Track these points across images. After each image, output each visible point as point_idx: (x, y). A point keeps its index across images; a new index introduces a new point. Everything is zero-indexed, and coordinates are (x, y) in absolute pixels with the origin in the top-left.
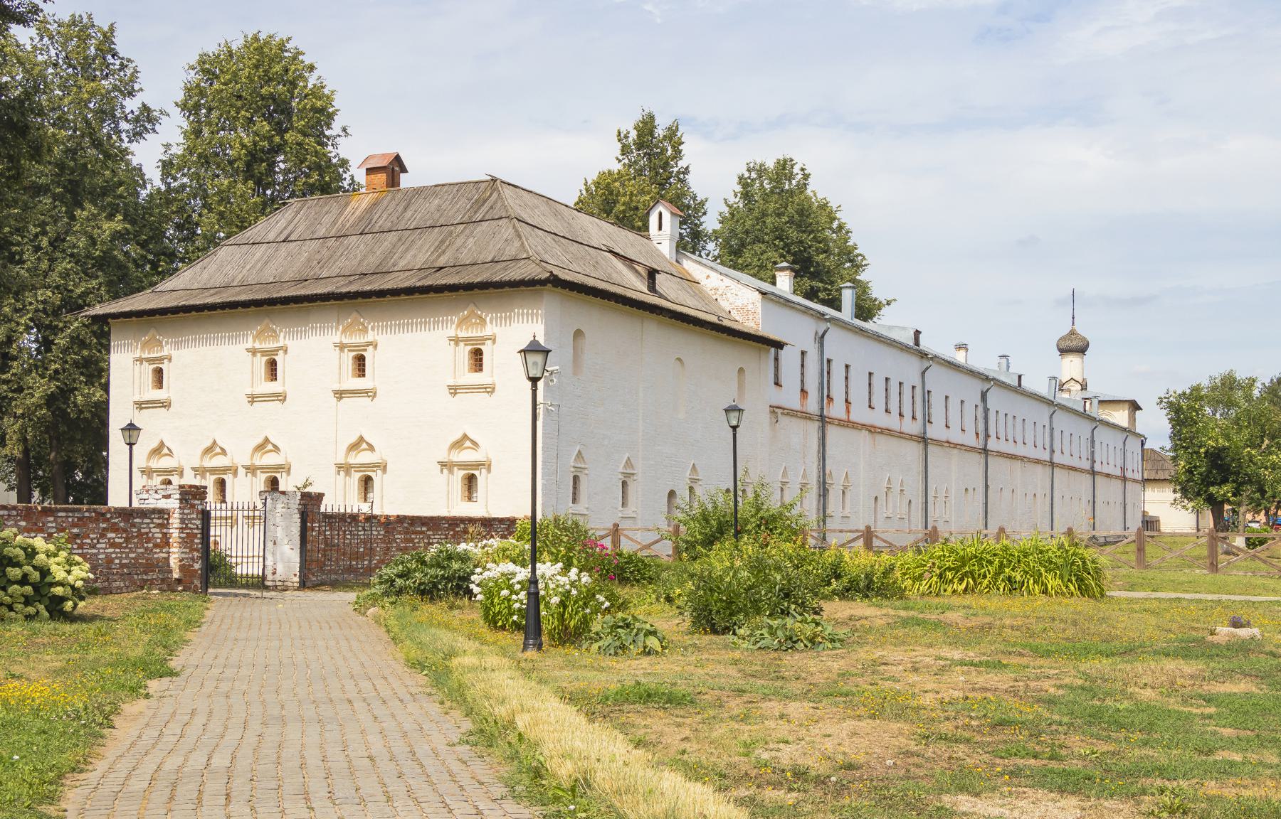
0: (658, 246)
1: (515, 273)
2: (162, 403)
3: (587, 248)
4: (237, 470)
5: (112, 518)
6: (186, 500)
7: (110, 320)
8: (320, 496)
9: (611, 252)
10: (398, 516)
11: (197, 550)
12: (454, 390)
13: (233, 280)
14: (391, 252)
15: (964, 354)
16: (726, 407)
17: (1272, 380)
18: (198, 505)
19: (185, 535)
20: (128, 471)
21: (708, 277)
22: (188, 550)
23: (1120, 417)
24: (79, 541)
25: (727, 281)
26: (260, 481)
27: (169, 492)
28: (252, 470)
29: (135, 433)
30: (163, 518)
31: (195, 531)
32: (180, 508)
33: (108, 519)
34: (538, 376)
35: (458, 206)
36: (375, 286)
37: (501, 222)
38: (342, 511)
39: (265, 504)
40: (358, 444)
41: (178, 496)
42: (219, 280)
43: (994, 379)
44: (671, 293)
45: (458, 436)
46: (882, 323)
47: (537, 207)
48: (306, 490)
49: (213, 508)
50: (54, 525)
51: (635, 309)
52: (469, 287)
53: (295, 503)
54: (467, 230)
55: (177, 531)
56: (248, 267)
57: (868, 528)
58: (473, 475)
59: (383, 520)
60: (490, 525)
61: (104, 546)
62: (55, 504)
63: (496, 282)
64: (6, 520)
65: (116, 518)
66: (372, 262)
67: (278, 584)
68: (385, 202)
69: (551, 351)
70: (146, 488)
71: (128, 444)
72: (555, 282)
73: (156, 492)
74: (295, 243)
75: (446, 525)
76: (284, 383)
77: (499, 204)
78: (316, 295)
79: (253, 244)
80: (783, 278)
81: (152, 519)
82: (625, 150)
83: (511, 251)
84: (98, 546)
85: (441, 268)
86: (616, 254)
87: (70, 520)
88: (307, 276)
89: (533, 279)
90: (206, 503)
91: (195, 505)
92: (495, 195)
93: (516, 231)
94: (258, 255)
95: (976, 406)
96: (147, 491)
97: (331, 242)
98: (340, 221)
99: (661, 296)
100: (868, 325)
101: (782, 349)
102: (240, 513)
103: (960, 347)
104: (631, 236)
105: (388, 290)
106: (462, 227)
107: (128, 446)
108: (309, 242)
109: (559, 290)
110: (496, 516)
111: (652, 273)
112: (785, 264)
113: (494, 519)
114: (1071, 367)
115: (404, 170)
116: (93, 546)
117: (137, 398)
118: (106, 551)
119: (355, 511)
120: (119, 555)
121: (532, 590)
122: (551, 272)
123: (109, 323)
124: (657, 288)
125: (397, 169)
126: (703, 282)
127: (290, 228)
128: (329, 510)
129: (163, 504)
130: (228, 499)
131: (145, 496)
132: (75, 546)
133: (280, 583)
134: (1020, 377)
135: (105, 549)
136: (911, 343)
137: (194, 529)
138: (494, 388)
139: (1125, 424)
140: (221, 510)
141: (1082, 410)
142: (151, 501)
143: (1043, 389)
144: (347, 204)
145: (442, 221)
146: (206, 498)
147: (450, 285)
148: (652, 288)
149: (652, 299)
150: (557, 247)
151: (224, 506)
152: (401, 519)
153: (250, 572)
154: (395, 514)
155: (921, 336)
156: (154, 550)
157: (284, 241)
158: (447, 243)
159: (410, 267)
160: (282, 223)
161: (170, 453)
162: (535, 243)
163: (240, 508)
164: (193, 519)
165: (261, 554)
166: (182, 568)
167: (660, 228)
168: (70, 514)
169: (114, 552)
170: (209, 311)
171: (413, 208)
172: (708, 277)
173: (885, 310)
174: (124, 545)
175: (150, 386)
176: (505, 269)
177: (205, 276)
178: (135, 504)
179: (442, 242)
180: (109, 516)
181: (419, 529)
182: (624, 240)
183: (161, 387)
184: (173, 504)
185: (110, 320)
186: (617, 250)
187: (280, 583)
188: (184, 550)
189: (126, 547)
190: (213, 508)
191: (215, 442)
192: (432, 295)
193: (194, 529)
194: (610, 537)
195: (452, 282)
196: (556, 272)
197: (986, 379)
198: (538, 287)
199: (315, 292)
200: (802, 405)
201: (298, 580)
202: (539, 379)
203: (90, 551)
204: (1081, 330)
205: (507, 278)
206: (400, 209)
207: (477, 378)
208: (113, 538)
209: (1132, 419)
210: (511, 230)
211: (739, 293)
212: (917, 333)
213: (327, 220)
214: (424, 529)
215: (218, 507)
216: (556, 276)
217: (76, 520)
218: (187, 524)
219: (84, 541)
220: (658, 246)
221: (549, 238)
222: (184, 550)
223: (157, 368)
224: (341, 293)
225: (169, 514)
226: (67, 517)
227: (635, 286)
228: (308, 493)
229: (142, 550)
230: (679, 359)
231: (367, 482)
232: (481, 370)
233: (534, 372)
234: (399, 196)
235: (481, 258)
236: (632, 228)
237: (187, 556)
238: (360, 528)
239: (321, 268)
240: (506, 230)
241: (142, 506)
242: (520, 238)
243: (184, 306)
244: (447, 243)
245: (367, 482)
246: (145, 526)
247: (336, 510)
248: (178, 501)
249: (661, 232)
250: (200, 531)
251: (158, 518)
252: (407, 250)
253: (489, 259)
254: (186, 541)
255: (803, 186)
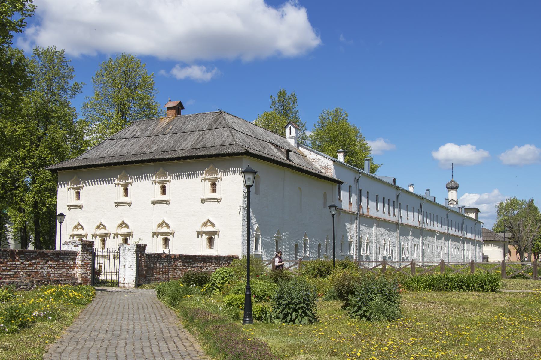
0: (290, 141)
1: (230, 150)
2: (79, 206)
3: (260, 141)
4: (110, 235)
5: (51, 255)
6: (85, 247)
7: (58, 171)
8: (145, 246)
9: (270, 143)
10: (179, 255)
11: (90, 270)
12: (203, 201)
13: (110, 154)
14: (177, 142)
15: (412, 188)
16: (330, 205)
17: (529, 200)
18: (90, 250)
19: (83, 263)
20: (61, 235)
21: (311, 154)
22: (85, 270)
23: (473, 215)
24: (35, 266)
25: (319, 156)
26: (120, 239)
27: (77, 244)
28: (116, 235)
29: (63, 217)
30: (74, 256)
31: (89, 261)
32: (82, 251)
33: (49, 256)
34: (251, 184)
35: (206, 123)
36: (170, 156)
37: (224, 129)
38: (155, 252)
39: (119, 249)
40: (163, 224)
41: (81, 246)
42: (104, 154)
43: (425, 199)
44: (295, 159)
45: (205, 220)
46: (378, 174)
47: (239, 123)
48: (139, 243)
49: (97, 251)
50: (24, 258)
51: (281, 166)
52: (210, 156)
53: (134, 249)
54: (210, 133)
55: (80, 261)
56: (116, 149)
57: (473, 261)
58: (212, 237)
59: (172, 257)
60: (219, 260)
61: (47, 268)
62: (36, 249)
63: (222, 154)
64: (1, 256)
65: (52, 255)
66: (169, 146)
67: (126, 285)
68: (175, 121)
69: (257, 172)
70: (67, 242)
71: (59, 222)
72: (248, 153)
73: (71, 244)
74: (136, 139)
75: (200, 259)
76: (131, 198)
77: (224, 121)
78: (145, 160)
79: (119, 139)
80: (340, 156)
81: (69, 256)
82: (273, 104)
83: (228, 141)
84: (44, 268)
85: (199, 148)
86: (273, 144)
87: (31, 256)
88: (141, 152)
89: (238, 152)
90: (94, 249)
91: (88, 250)
92: (222, 118)
93: (231, 132)
94: (121, 144)
95: (419, 210)
96: (67, 243)
97: (152, 138)
98: (156, 130)
99: (291, 161)
100: (373, 175)
101: (342, 184)
102: (111, 253)
103: (410, 186)
104: (279, 137)
105: (176, 158)
106: (208, 131)
107: (60, 223)
108: (142, 138)
109: (249, 157)
110: (222, 255)
111: (288, 151)
112: (341, 150)
113: (221, 256)
114: (452, 195)
115: (183, 108)
116: (42, 268)
117: (69, 204)
118: (48, 270)
119: (162, 253)
120: (54, 272)
121: (248, 293)
122: (246, 150)
123: (57, 173)
124: (290, 158)
125: (180, 107)
126: (309, 156)
127: (134, 132)
128: (149, 252)
129: (74, 249)
130: (106, 248)
131: (67, 246)
132: (34, 268)
133: (127, 285)
134: (435, 198)
135: (47, 269)
136: (392, 183)
137: (88, 260)
138: (221, 200)
139: (474, 218)
140: (103, 252)
141: (459, 212)
142: (69, 248)
143: (443, 203)
144: (159, 122)
145: (199, 129)
146: (93, 246)
147: (204, 155)
148: (288, 157)
149: (288, 162)
150: (248, 140)
151: (104, 250)
152: (181, 256)
153: (113, 279)
154: (178, 254)
155: (396, 181)
156: (70, 270)
157: (132, 138)
158: (201, 138)
159: (185, 148)
160: (131, 130)
161: (82, 228)
162: (239, 138)
163: (111, 251)
164: (88, 256)
165: (118, 271)
166: (82, 278)
167: (290, 134)
168: (32, 254)
169: (51, 271)
170: (100, 167)
171: (186, 124)
172: (311, 154)
173: (379, 169)
174: (56, 268)
175: (74, 200)
176: (226, 149)
177: (98, 153)
178: (62, 249)
179: (199, 138)
180: (49, 254)
181: (189, 261)
182: (276, 138)
183: (79, 200)
184: (79, 249)
185: (58, 171)
186: (273, 142)
187: (127, 285)
188: (84, 270)
189: (57, 269)
190: (97, 251)
191: (101, 223)
192: (194, 160)
193: (88, 260)
194: (271, 264)
195: (203, 154)
196: (248, 149)
197: (422, 198)
198: (240, 156)
199: (144, 159)
200: (350, 208)
201: (135, 283)
202: (251, 186)
203: (40, 270)
204: (456, 180)
205: (227, 152)
206: (181, 124)
207: (214, 196)
208: (51, 265)
209: (477, 216)
210: (228, 131)
211: (324, 161)
212: (395, 179)
213: (150, 129)
214: (191, 261)
215: (101, 251)
216: (248, 151)
217: (34, 256)
218: (85, 258)
219: (38, 266)
220: (290, 141)
221: (244, 136)
222: (84, 270)
223: (77, 191)
224: (155, 159)
225: (77, 254)
226: (30, 255)
227: (281, 157)
228: (139, 244)
229: (65, 270)
230: (299, 188)
231: (166, 241)
232: (216, 192)
233: (249, 183)
234: (181, 118)
235: (216, 144)
236: (279, 134)
237: (84, 272)
238: (162, 260)
239: (147, 149)
240: (226, 132)
241: (65, 250)
242: (233, 136)
243: (89, 165)
244: (201, 138)
245: (166, 241)
246: (66, 259)
247: (153, 252)
248: (81, 248)
249: (291, 135)
250: (91, 261)
251: (72, 256)
252: (184, 141)
253: (219, 144)
254: (85, 266)
255: (345, 120)
